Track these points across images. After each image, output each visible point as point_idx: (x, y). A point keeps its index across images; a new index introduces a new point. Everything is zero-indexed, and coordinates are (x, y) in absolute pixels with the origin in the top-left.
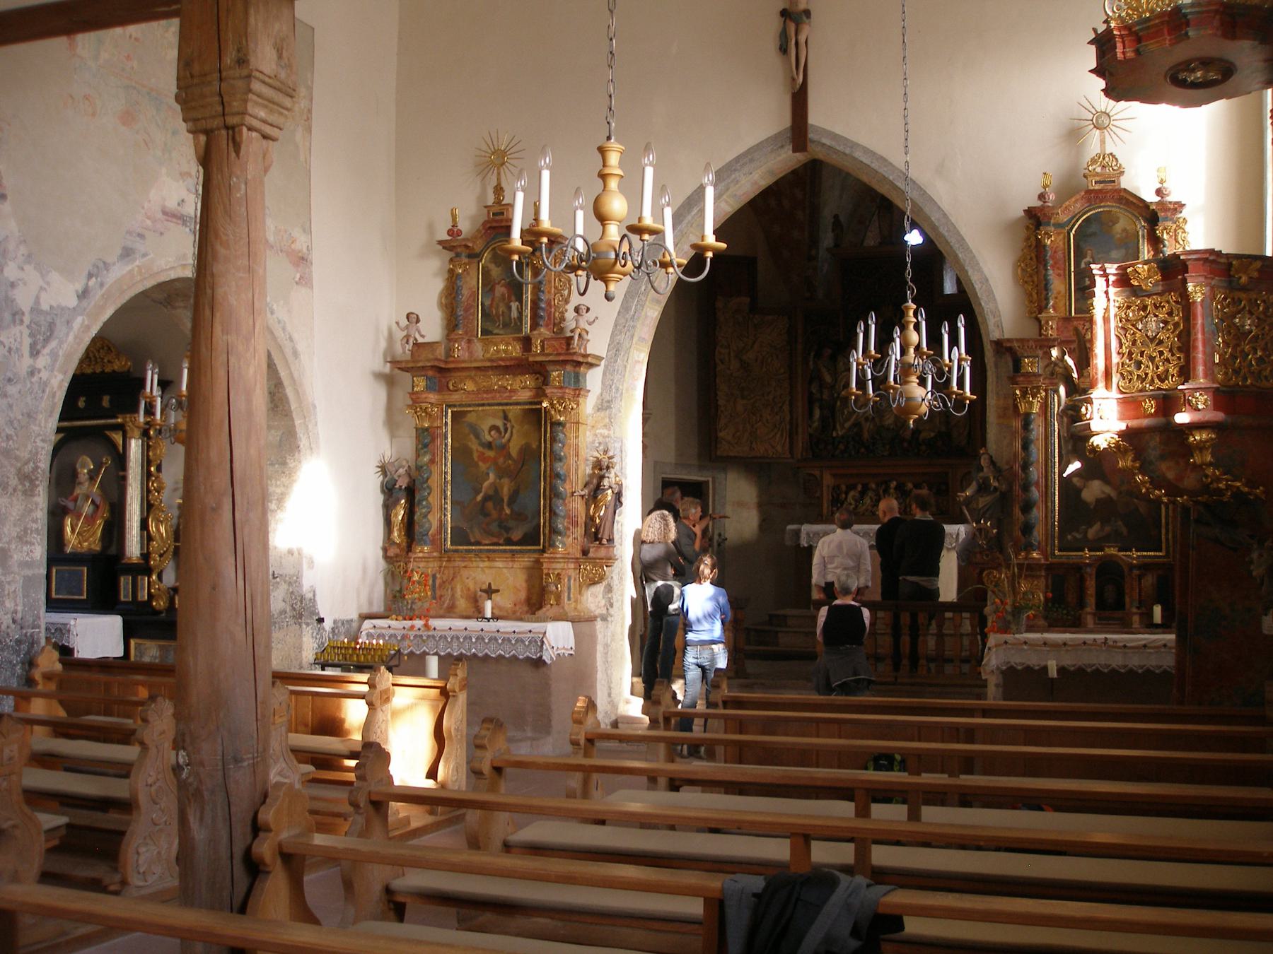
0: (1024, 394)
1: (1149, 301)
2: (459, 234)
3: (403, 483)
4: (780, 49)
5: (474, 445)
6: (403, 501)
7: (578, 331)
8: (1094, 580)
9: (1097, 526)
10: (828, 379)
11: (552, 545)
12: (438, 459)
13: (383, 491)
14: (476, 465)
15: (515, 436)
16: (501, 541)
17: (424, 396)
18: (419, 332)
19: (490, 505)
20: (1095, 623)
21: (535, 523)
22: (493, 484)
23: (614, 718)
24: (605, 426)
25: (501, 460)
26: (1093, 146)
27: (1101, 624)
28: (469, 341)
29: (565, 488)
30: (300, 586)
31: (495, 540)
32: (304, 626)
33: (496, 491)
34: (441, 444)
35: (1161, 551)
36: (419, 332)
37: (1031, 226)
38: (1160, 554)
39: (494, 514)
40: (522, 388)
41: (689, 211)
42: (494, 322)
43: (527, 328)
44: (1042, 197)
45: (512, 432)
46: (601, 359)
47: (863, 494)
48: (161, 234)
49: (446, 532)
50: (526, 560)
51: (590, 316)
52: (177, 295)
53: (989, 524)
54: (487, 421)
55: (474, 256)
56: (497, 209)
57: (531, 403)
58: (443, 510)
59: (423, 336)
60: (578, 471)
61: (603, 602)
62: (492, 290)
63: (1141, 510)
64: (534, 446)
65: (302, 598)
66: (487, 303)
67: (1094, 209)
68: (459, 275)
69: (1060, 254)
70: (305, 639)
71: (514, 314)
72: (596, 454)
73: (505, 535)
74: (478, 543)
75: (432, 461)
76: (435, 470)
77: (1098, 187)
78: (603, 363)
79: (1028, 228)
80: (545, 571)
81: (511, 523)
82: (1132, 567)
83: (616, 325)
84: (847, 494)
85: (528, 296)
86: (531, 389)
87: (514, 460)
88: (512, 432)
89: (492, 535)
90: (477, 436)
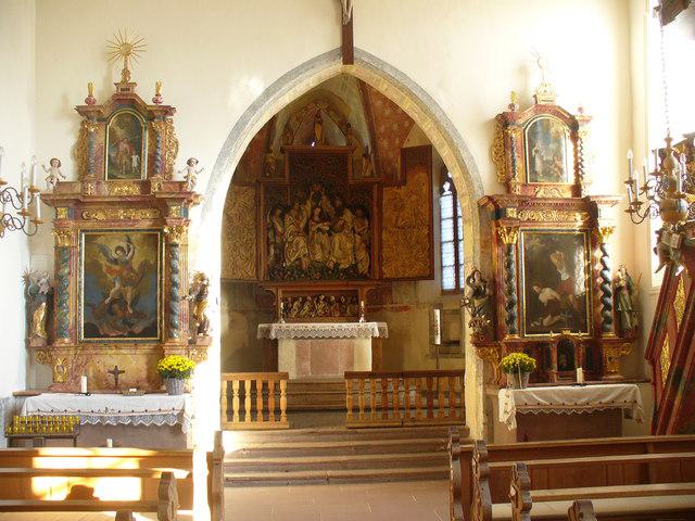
0: (509, 231)
3: (45, 289)
5: (103, 261)
6: (44, 304)
10: (280, 229)
11: (171, 336)
13: (26, 296)
14: (105, 276)
15: (136, 255)
19: (116, 307)
21: (153, 319)
22: (119, 290)
28: (98, 183)
29: (179, 293)
39: (120, 314)
40: (144, 219)
42: (117, 170)
43: (144, 175)
44: (512, 106)
47: (303, 303)
50: (147, 348)
51: (197, 167)
54: (114, 244)
55: (103, 120)
58: (77, 310)
60: (185, 281)
64: (152, 262)
66: (113, 155)
68: (91, 133)
71: (135, 164)
74: (108, 336)
77: (543, 103)
81: (133, 320)
82: (579, 343)
84: (293, 303)
85: (146, 152)
90: (106, 254)
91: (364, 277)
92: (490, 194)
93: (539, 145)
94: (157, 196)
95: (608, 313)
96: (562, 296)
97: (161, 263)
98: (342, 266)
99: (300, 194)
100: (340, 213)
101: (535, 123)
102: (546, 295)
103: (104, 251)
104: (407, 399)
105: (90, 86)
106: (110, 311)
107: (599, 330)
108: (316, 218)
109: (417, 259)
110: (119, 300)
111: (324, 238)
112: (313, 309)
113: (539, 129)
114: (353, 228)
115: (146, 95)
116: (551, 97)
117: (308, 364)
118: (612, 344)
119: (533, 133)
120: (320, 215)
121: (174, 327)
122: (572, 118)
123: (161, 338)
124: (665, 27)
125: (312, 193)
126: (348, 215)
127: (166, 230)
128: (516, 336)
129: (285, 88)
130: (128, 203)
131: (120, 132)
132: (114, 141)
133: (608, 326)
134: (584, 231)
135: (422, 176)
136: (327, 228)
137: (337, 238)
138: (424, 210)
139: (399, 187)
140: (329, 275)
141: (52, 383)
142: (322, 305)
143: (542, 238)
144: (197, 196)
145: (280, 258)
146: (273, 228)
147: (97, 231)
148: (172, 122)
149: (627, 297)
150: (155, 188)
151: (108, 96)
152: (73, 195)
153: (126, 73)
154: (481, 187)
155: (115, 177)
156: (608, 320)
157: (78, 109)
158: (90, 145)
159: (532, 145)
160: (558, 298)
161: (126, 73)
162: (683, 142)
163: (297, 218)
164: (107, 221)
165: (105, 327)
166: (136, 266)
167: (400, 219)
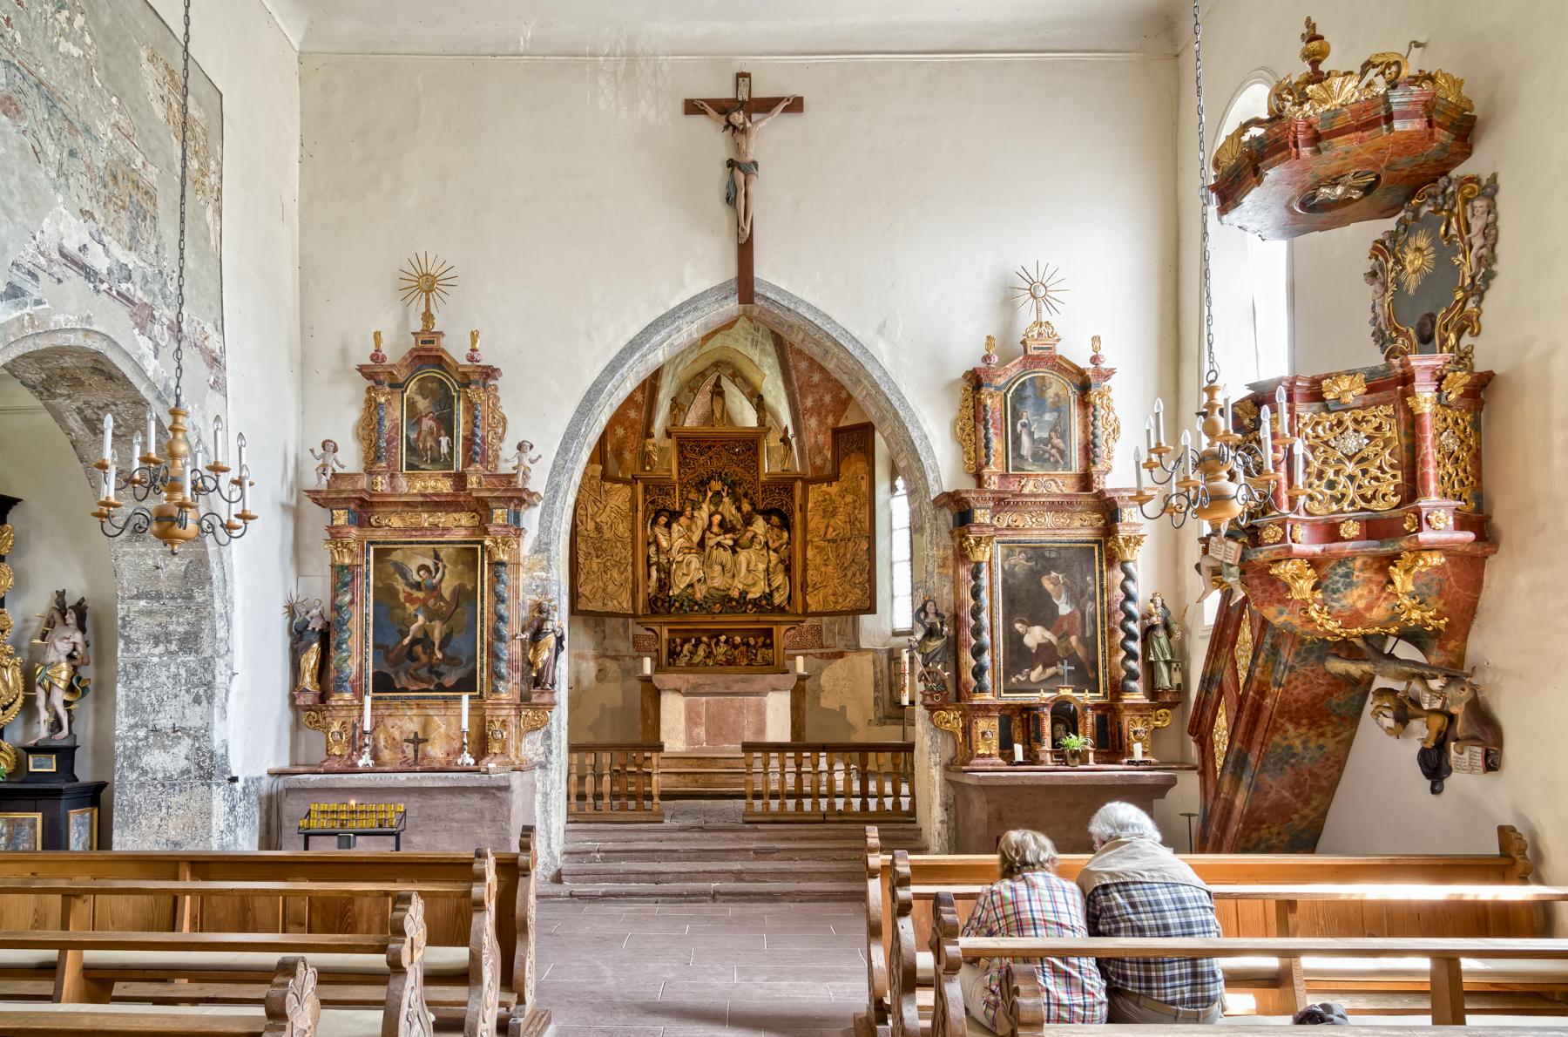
0: (978, 543)
1: (1347, 417)
2: (384, 359)
3: (316, 625)
4: (728, 199)
5: (400, 586)
6: (316, 645)
7: (522, 468)
9: (1040, 668)
10: (664, 544)
12: (357, 599)
13: (291, 633)
14: (403, 607)
15: (447, 576)
16: (432, 688)
17: (346, 530)
18: (337, 462)
19: (418, 649)
22: (422, 626)
23: (554, 870)
24: (543, 569)
25: (431, 602)
26: (1026, 317)
28: (392, 476)
30: (210, 740)
31: (425, 686)
32: (214, 787)
33: (426, 634)
34: (362, 583)
36: (337, 462)
39: (424, 658)
40: (458, 525)
41: (632, 355)
43: (458, 464)
44: (986, 358)
45: (444, 573)
46: (540, 498)
47: (696, 646)
48: (60, 281)
49: (367, 677)
51: (532, 454)
52: (62, 377)
55: (397, 386)
56: (426, 337)
57: (466, 542)
59: (342, 467)
60: (517, 615)
61: (541, 750)
62: (419, 422)
64: (469, 587)
65: (212, 755)
68: (380, 404)
69: (997, 415)
70: (215, 802)
71: (444, 449)
72: (534, 597)
73: (437, 681)
74: (405, 690)
75: (352, 602)
76: (356, 610)
77: (1036, 353)
78: (540, 503)
80: (488, 718)
81: (443, 668)
82: (1085, 707)
83: (554, 466)
84: (682, 646)
85: (460, 431)
86: (466, 528)
87: (446, 602)
88: (444, 573)
89: (422, 681)
90: (404, 576)
91: (781, 610)
92: (951, 490)
93: (1027, 415)
94: (474, 494)
95: (1132, 664)
97: (482, 588)
98: (750, 596)
99: (693, 496)
100: (748, 521)
101: (1023, 383)
102: (1035, 636)
103: (402, 571)
104: (831, 783)
105: (377, 335)
106: (410, 655)
107: (1118, 689)
108: (715, 529)
109: (854, 586)
110: (424, 640)
111: (726, 556)
112: (709, 654)
113: (1029, 391)
114: (767, 543)
115: (456, 349)
117: (701, 731)
118: (1138, 710)
119: (1019, 398)
120: (721, 524)
121: (500, 677)
122: (1081, 372)
123: (481, 692)
124: (1225, 217)
125: (710, 494)
126: (759, 526)
127: (487, 542)
129: (656, 339)
130: (435, 504)
131: (422, 404)
132: (415, 417)
133: (1132, 684)
134: (1096, 542)
135: (860, 467)
136: (731, 543)
137: (743, 556)
138: (864, 515)
139: (830, 483)
140: (732, 607)
141: (325, 757)
142: (722, 649)
143: (1030, 553)
144: (531, 494)
145: (664, 585)
146: (657, 543)
147: (391, 543)
148: (496, 389)
149: (1163, 641)
150: (472, 482)
151: (404, 351)
152: (354, 491)
153: (428, 317)
154: (938, 480)
155: (417, 468)
156: (1132, 675)
157: (361, 369)
158: (380, 421)
159: (1016, 416)
160: (1054, 639)
161: (428, 317)
162: (1249, 397)
163: (689, 529)
164: (405, 530)
165: (402, 675)
166: (446, 593)
167: (831, 529)
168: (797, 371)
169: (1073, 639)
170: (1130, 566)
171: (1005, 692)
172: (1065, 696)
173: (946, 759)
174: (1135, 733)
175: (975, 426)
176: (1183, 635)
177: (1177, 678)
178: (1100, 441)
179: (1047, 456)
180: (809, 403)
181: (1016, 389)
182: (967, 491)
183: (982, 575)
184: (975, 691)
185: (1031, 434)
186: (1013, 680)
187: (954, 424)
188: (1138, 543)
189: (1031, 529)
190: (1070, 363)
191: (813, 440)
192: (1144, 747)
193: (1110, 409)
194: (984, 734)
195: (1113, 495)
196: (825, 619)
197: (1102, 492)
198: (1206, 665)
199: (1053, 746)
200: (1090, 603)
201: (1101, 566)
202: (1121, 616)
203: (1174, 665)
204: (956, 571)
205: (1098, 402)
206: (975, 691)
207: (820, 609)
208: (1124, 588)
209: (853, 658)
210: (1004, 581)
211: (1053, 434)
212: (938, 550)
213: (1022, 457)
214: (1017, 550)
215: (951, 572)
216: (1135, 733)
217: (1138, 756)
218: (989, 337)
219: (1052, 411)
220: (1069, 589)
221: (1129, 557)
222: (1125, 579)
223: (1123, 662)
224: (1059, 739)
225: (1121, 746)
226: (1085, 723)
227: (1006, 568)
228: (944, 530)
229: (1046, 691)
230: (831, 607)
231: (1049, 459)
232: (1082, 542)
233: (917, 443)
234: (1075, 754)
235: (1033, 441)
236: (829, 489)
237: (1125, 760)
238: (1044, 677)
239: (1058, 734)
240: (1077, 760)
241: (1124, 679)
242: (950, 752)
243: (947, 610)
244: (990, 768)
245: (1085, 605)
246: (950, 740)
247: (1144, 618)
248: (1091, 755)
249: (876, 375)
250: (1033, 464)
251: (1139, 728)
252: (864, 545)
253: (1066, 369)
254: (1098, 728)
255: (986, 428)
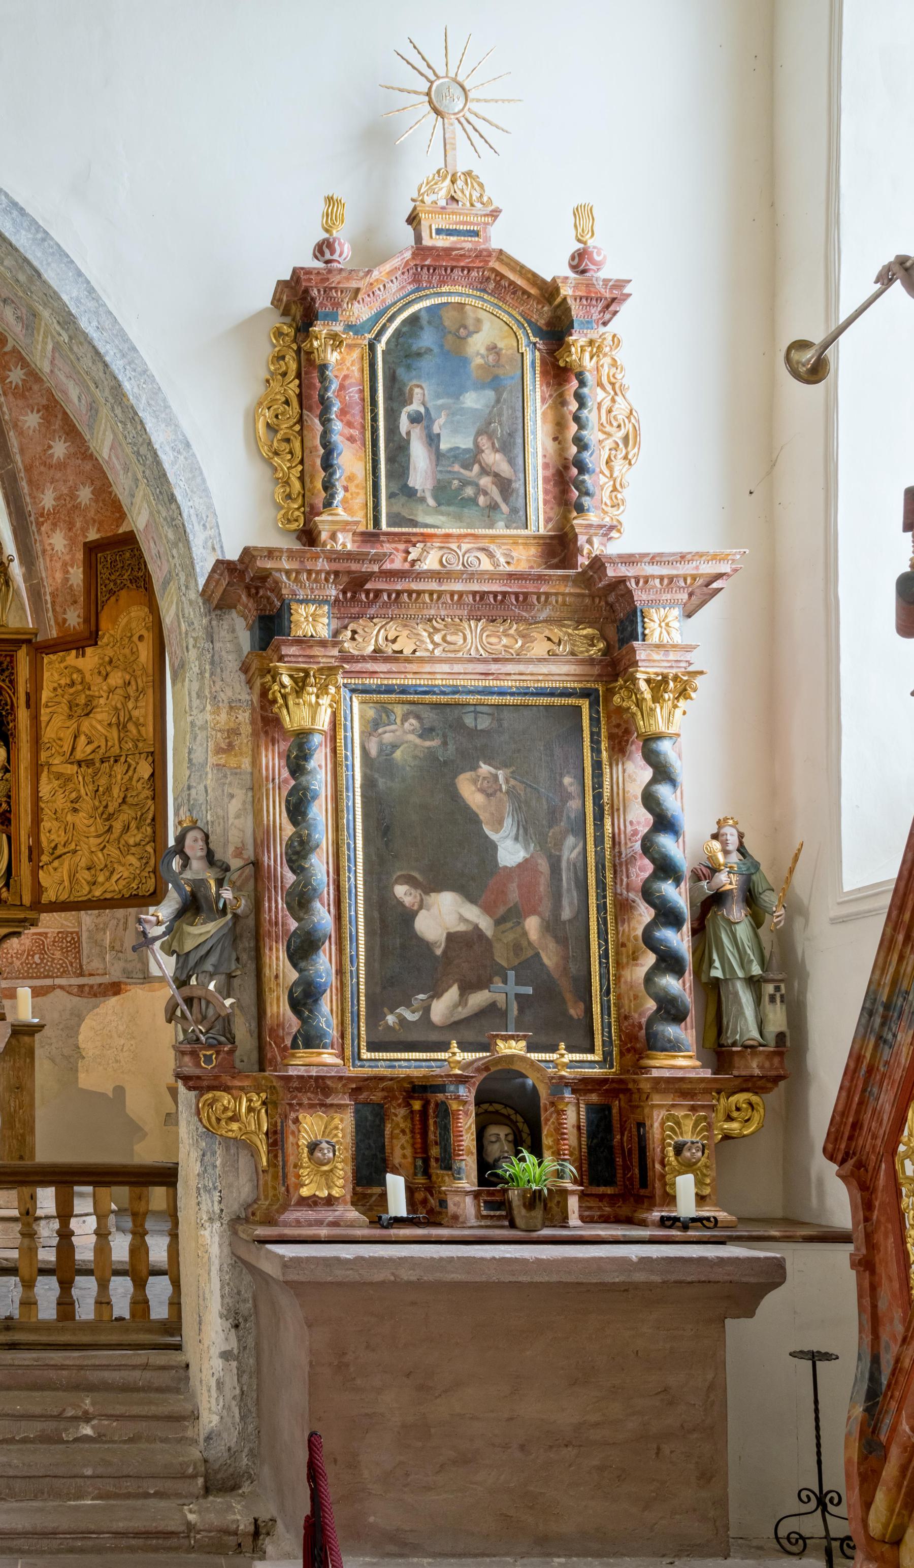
0: (300, 685)
8: (542, 1105)
9: (453, 993)
20: (480, 1217)
27: (491, 1217)
35: (592, 1051)
37: (286, 329)
38: (590, 1057)
44: (323, 248)
53: (211, 987)
63: (546, 961)
67: (427, 297)
69: (353, 393)
77: (442, 242)
79: (279, 334)
82: (559, 1084)
96: (498, 922)
101: (414, 320)
113: (427, 339)
116: (473, 221)
128: (328, 1057)
133: (671, 1031)
134: (585, 694)
138: (143, 711)
143: (430, 716)
149: (743, 931)
160: (485, 924)
167: (82, 740)
168: (21, 433)
169: (532, 925)
170: (665, 746)
171: (372, 1047)
172: (511, 1058)
173: (234, 1207)
174: (679, 1149)
175: (301, 421)
176: (789, 920)
177: (777, 1019)
178: (595, 459)
179: (469, 491)
180: (48, 500)
181: (398, 333)
182: (271, 553)
183: (312, 764)
184: (294, 1045)
185: (432, 440)
186: (391, 1019)
187: (252, 419)
188: (683, 693)
189: (432, 660)
190: (522, 270)
191: (59, 575)
192: (699, 1183)
193: (617, 389)
194: (313, 1147)
195: (623, 571)
196: (88, 918)
197: (597, 564)
198: (880, 966)
199: (482, 1181)
200: (571, 840)
201: (596, 750)
202: (644, 869)
203: (770, 988)
204: (255, 762)
205: (588, 363)
206: (294, 1045)
207: (63, 897)
208: (650, 800)
209: (137, 994)
210: (369, 784)
211: (484, 441)
212: (216, 711)
213: (410, 493)
214: (399, 710)
215: (246, 764)
216: (679, 1149)
217: (686, 1207)
218: (330, 200)
219: (480, 386)
220: (520, 805)
221: (662, 727)
222: (654, 781)
223: (649, 979)
224: (495, 1164)
225: (644, 1181)
226: (559, 1129)
227: (373, 751)
228: (232, 663)
229: (464, 1047)
230: (83, 892)
231: (474, 501)
232: (552, 694)
233: (166, 459)
234: (534, 1200)
235: (438, 456)
236: (80, 663)
237: (656, 1215)
238: (463, 1013)
239: (494, 1151)
240: (538, 1213)
241: (650, 1022)
242: (243, 1189)
243: (238, 853)
244: (323, 1232)
245: (559, 844)
246: (244, 1161)
247: (697, 877)
248: (573, 1203)
249: (69, 294)
250: (437, 511)
251: (688, 1138)
252: (145, 770)
253: (514, 288)
254: (591, 1135)
255: (326, 422)
